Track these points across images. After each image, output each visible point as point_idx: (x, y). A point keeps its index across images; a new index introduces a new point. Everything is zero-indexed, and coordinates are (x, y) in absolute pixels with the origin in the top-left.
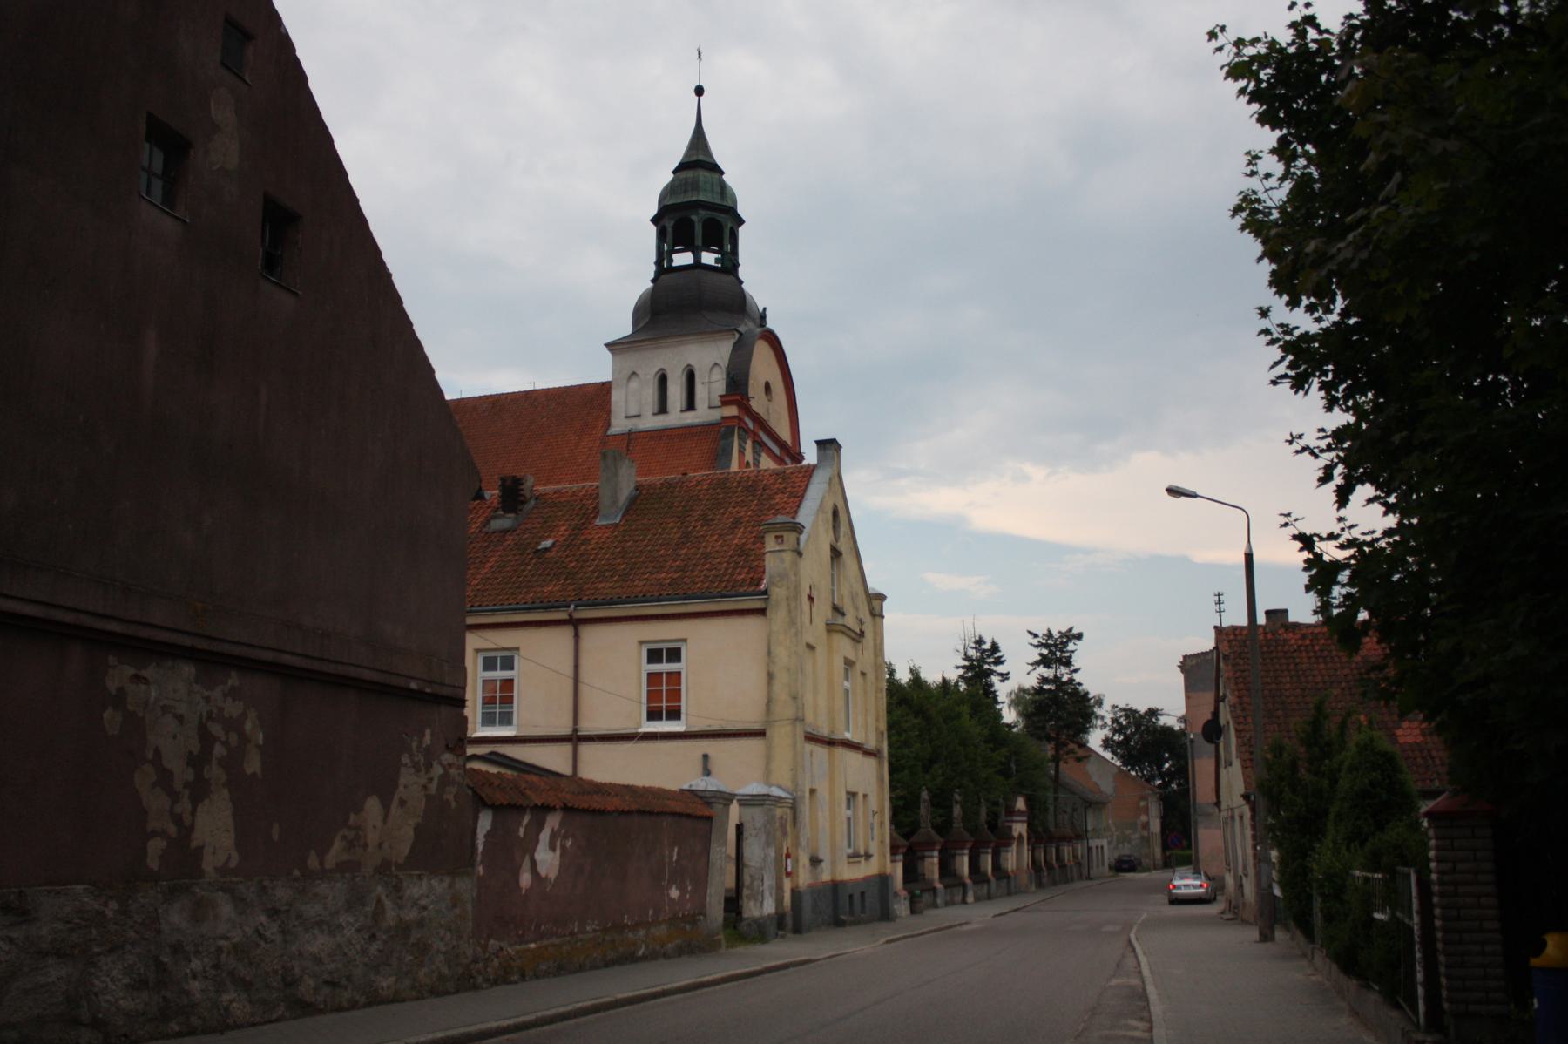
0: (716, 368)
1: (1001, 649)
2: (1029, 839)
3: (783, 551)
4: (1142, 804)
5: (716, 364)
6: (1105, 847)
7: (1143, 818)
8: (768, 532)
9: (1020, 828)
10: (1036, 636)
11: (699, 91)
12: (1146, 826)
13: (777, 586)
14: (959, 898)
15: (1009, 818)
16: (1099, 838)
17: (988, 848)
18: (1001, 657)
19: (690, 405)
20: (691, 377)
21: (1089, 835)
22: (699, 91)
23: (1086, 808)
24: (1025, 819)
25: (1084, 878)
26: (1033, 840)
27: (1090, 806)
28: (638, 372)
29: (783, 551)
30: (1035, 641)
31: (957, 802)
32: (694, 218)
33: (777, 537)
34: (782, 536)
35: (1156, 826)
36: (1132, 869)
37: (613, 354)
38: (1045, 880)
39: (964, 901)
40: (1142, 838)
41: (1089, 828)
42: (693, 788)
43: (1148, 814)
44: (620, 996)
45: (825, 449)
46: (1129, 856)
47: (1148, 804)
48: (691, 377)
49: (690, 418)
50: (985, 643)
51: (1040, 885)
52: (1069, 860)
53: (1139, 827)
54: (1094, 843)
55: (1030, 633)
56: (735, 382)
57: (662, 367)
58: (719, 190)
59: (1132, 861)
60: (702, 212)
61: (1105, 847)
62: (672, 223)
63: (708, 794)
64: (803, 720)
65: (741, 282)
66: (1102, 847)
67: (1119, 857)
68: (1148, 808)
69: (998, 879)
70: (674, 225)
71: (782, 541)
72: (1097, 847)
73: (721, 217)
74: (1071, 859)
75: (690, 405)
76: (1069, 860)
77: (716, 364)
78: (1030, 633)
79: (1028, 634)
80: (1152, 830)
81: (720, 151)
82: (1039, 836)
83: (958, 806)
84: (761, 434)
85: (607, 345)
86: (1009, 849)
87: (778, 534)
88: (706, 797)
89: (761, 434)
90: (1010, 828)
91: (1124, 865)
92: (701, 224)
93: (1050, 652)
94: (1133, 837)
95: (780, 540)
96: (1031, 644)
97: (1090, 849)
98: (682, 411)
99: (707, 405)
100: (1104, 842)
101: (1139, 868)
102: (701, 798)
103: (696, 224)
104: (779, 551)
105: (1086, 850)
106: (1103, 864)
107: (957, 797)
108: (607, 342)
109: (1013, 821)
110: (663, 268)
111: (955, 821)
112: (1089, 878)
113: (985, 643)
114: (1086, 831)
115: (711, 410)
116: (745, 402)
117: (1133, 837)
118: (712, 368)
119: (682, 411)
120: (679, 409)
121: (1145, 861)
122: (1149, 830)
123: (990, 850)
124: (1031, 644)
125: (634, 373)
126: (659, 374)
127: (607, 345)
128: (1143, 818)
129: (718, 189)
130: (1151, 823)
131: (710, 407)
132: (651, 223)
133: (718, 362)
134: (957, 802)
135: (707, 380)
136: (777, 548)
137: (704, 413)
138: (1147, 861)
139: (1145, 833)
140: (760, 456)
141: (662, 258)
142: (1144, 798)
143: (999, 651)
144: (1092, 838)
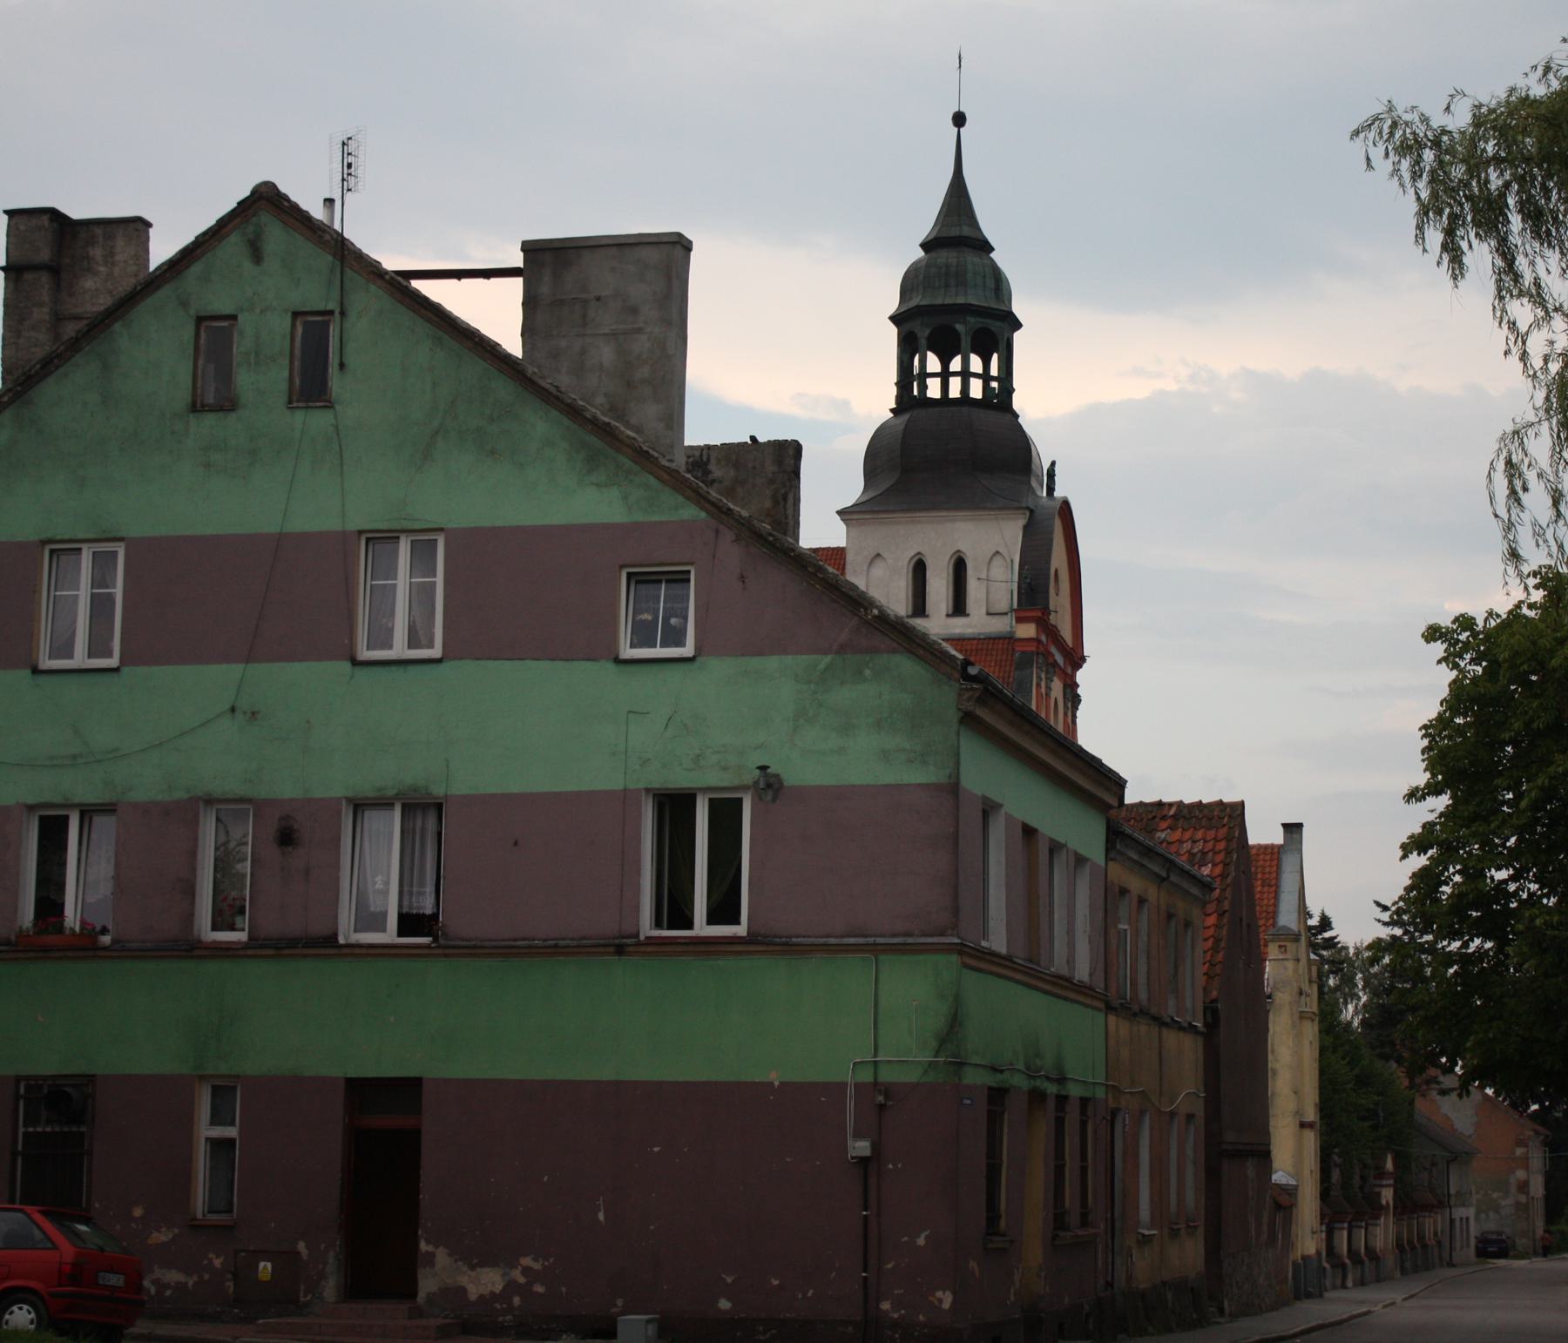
0: (998, 558)
1: (1334, 925)
2: (1395, 1207)
3: (1286, 959)
4: (1519, 1151)
5: (997, 552)
6: (1471, 1219)
7: (1521, 1174)
8: (1272, 941)
9: (1387, 1195)
10: (1385, 908)
11: (959, 120)
12: (1523, 1187)
13: (1281, 992)
14: (1339, 1282)
15: (1378, 1182)
16: (1463, 1205)
17: (1343, 1222)
18: (1335, 937)
19: (959, 607)
20: (959, 568)
21: (1452, 1203)
22: (959, 120)
23: (1448, 1163)
24: (1391, 1182)
25: (1445, 1264)
26: (1399, 1210)
27: (1455, 1159)
28: (881, 553)
29: (1286, 959)
30: (1386, 917)
31: (1336, 1165)
32: (959, 327)
33: (1280, 947)
34: (1285, 946)
35: (1537, 1188)
36: (1503, 1254)
37: (847, 525)
38: (1408, 1265)
39: (1344, 1286)
40: (1517, 1204)
41: (1452, 1191)
42: (1278, 1182)
43: (1527, 1168)
44: (1355, 1313)
45: (1291, 833)
46: (1499, 1233)
47: (1528, 1151)
48: (959, 568)
49: (959, 626)
50: (1311, 916)
51: (1404, 1272)
52: (1430, 1239)
53: (1513, 1189)
54: (1459, 1213)
55: (1378, 904)
56: (1032, 590)
57: (920, 549)
58: (993, 286)
59: (1503, 1241)
60: (971, 320)
61: (1471, 1219)
62: (927, 332)
63: (1289, 1187)
64: (1297, 1112)
65: (1017, 416)
66: (1467, 1219)
67: (1483, 1234)
68: (1527, 1159)
69: (1371, 1259)
70: (931, 333)
71: (1286, 950)
72: (1461, 1219)
73: (995, 326)
74: (1432, 1237)
75: (959, 607)
76: (1430, 1239)
77: (997, 552)
78: (1378, 904)
79: (1374, 905)
80: (1532, 1194)
81: (990, 223)
82: (1408, 1205)
83: (1338, 1170)
84: (1053, 650)
85: (839, 513)
86: (1378, 1222)
87: (1282, 944)
88: (1289, 1189)
89: (1053, 650)
90: (1379, 1194)
91: (1492, 1248)
92: (969, 339)
93: (1406, 932)
94: (1503, 1203)
95: (1283, 949)
96: (1379, 921)
97: (1452, 1221)
98: (948, 615)
99: (984, 611)
100: (1470, 1212)
101: (1511, 1253)
102: (1283, 1190)
103: (963, 337)
104: (1283, 959)
105: (1448, 1223)
106: (1468, 1246)
107: (1495, 1195)
108: (839, 509)
109: (1382, 1186)
110: (908, 400)
111: (1333, 1187)
112: (1451, 1265)
113: (1311, 916)
114: (1449, 1195)
115: (990, 617)
116: (1046, 617)
117: (1503, 1203)
118: (994, 555)
119: (948, 615)
120: (944, 612)
121: (1522, 1243)
122: (1527, 1193)
123: (1346, 1225)
124: (1379, 921)
125: (878, 555)
126: (917, 558)
127: (839, 513)
128: (1521, 1174)
129: (991, 283)
130: (1532, 1183)
131: (988, 614)
132: (889, 321)
133: (1001, 550)
134: (1336, 1165)
135: (984, 576)
136: (1281, 957)
137: (976, 623)
138: (1524, 1241)
139: (1523, 1198)
140: (1052, 681)
141: (907, 378)
142: (1521, 1143)
143: (787, 455)
144: (1456, 1206)
